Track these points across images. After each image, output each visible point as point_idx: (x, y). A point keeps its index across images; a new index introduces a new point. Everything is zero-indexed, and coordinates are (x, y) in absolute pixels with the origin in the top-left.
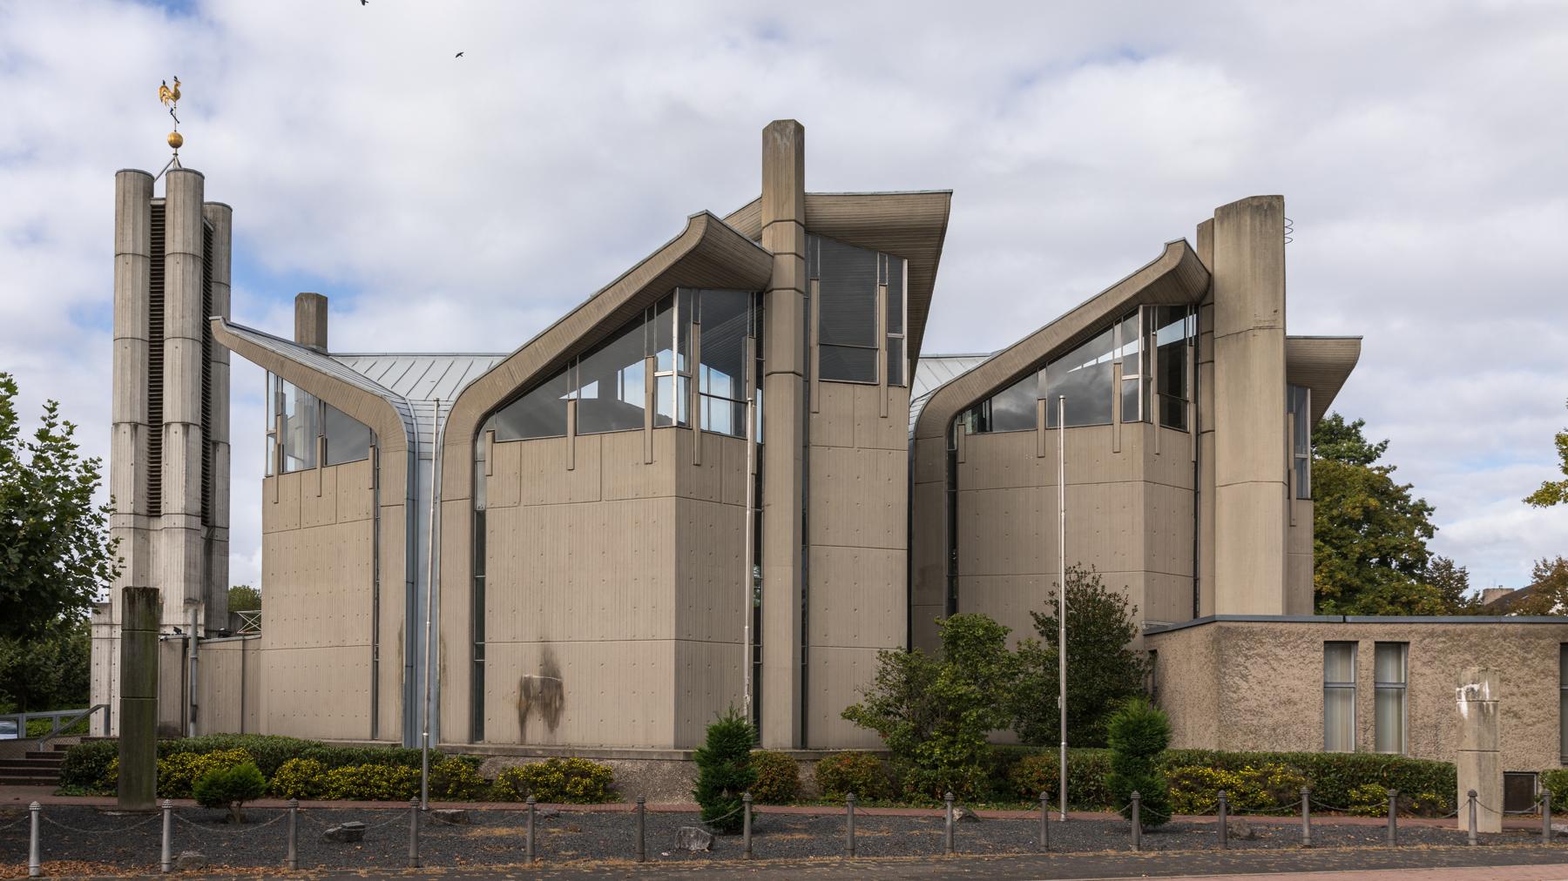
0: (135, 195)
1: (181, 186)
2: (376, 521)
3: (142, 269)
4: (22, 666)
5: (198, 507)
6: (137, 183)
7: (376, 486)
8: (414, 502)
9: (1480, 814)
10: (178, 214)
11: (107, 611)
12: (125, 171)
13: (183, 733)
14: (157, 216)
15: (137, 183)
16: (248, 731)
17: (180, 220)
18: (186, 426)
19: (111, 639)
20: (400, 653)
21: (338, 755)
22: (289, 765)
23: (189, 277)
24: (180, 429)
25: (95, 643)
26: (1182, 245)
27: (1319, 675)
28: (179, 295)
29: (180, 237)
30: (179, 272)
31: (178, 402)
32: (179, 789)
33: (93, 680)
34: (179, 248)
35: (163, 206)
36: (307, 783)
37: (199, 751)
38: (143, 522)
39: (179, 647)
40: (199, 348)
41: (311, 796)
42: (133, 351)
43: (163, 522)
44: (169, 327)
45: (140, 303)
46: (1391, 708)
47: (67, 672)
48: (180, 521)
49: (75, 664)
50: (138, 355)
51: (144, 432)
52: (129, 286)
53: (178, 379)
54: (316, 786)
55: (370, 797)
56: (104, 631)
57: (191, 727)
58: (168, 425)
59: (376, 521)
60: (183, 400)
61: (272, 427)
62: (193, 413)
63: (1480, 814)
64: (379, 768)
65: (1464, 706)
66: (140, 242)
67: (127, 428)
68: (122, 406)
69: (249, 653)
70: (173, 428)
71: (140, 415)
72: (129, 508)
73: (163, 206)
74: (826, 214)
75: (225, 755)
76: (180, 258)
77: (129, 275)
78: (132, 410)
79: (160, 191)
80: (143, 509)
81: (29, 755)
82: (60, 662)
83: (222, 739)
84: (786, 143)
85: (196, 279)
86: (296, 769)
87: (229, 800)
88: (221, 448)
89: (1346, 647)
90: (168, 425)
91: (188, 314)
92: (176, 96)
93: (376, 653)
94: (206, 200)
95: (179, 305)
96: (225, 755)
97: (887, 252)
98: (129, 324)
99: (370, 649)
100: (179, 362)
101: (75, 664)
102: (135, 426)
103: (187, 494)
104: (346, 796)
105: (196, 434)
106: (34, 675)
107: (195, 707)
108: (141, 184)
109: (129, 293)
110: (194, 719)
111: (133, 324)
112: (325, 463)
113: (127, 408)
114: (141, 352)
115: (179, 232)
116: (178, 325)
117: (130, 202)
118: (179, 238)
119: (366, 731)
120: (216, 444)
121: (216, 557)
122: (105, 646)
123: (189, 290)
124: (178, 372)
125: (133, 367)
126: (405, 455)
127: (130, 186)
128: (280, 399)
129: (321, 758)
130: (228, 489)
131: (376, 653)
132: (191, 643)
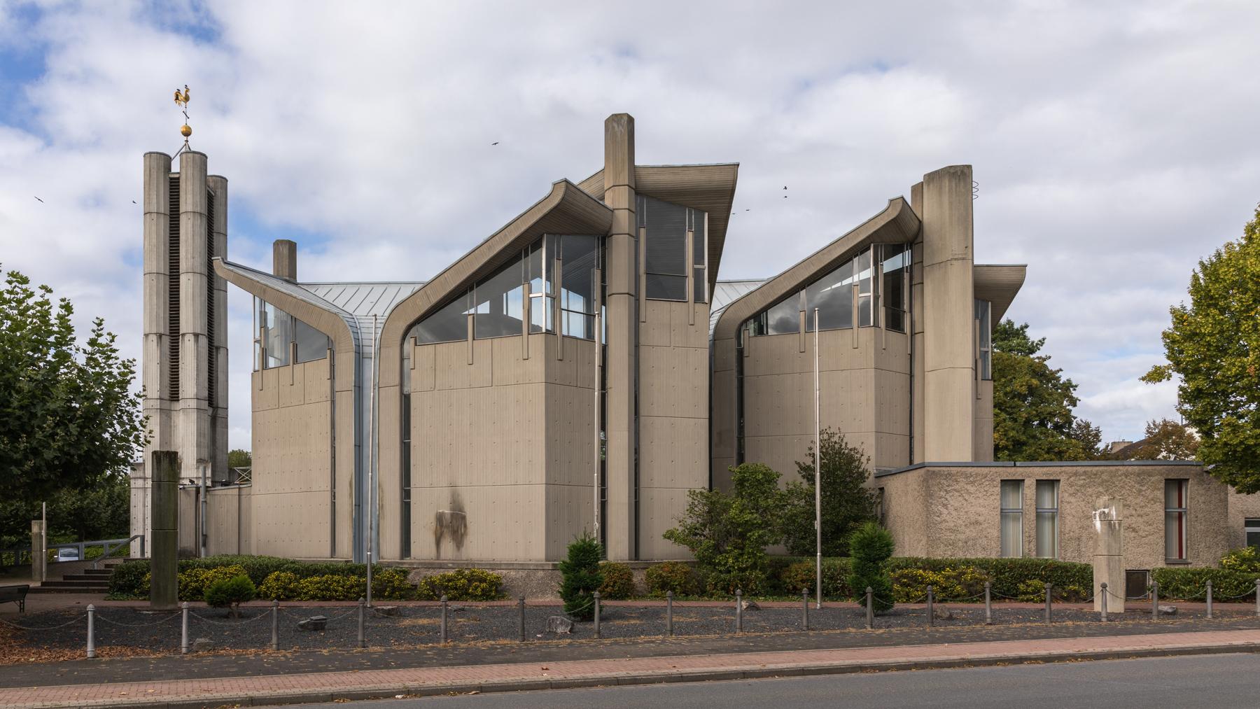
1: (191, 164)
2: (333, 402)
3: (164, 223)
4: (81, 508)
5: (206, 394)
7: (332, 377)
8: (359, 388)
9: (1109, 599)
10: (189, 183)
13: (197, 555)
14: (174, 185)
16: (243, 552)
17: (190, 188)
18: (196, 335)
19: (145, 489)
20: (351, 495)
21: (307, 569)
22: (272, 576)
23: (197, 229)
24: (192, 338)
25: (133, 492)
27: (998, 504)
28: (190, 241)
29: (190, 201)
30: (190, 225)
31: (190, 318)
32: (193, 595)
34: (190, 208)
36: (285, 589)
37: (208, 567)
38: (167, 405)
39: (193, 494)
40: (205, 280)
41: (288, 598)
42: (158, 282)
43: (181, 405)
44: (184, 265)
45: (162, 247)
46: (1047, 526)
48: (193, 404)
51: (166, 340)
52: (154, 236)
53: (190, 302)
54: (291, 591)
55: (330, 598)
56: (140, 483)
57: (203, 550)
59: (333, 402)
60: (194, 317)
61: (257, 336)
62: (201, 327)
63: (1109, 599)
64: (336, 577)
65: (1098, 524)
67: (154, 338)
68: (151, 322)
70: (187, 337)
71: (164, 328)
72: (156, 395)
74: (649, 180)
75: (227, 570)
76: (190, 215)
77: (154, 228)
78: (158, 325)
79: (175, 167)
80: (167, 396)
83: (224, 559)
84: (621, 130)
86: (277, 579)
87: (229, 603)
88: (222, 351)
89: (1014, 484)
91: (197, 256)
92: (187, 99)
93: (334, 496)
94: (209, 173)
95: (190, 249)
96: (227, 570)
97: (694, 206)
98: (154, 263)
99: (329, 494)
100: (190, 290)
102: (160, 336)
103: (198, 384)
104: (313, 598)
105: (204, 341)
107: (205, 536)
108: (162, 163)
109: (154, 241)
110: (204, 545)
111: (158, 263)
112: (296, 361)
113: (154, 324)
114: (164, 283)
115: (190, 196)
116: (190, 264)
117: (154, 175)
118: (190, 201)
120: (218, 348)
121: (219, 429)
122: (140, 494)
124: (190, 297)
126: (353, 355)
127: (154, 164)
128: (264, 316)
129: (295, 571)
131: (334, 496)
132: (202, 490)
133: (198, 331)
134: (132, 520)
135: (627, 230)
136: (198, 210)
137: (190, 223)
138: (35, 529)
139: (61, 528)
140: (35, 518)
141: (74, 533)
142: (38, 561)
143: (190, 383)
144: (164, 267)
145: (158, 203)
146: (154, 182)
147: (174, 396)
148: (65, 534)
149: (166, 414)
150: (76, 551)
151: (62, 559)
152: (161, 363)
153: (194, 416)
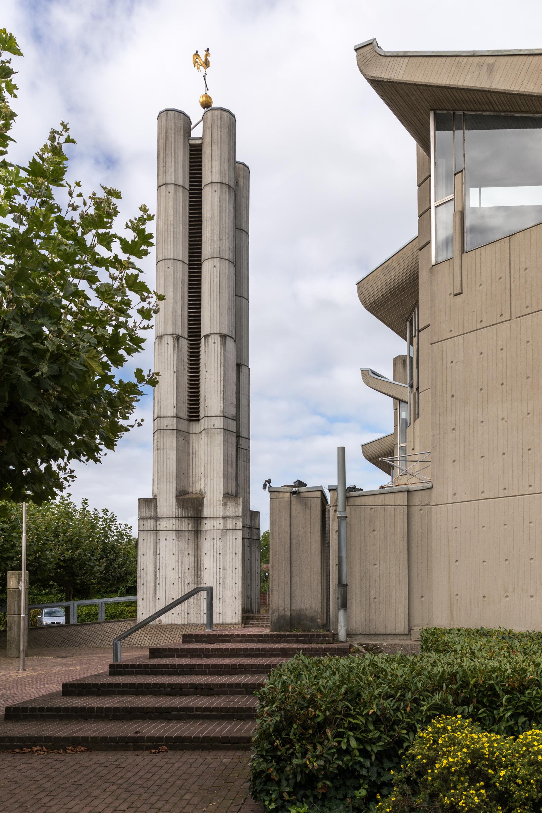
0: (177, 132)
1: (217, 123)
3: (182, 199)
4: (72, 560)
5: (232, 411)
6: (174, 122)
10: (216, 148)
11: (152, 505)
12: (167, 110)
14: (195, 153)
15: (174, 122)
17: (216, 153)
18: (223, 337)
23: (225, 204)
24: (218, 339)
26: (319, 494)
28: (216, 219)
29: (212, 171)
31: (212, 319)
33: (139, 569)
34: (216, 179)
35: (201, 145)
38: (184, 425)
42: (175, 271)
43: (203, 424)
44: (208, 247)
45: (180, 228)
47: (107, 568)
48: (219, 423)
49: (114, 560)
50: (179, 274)
51: (184, 344)
52: (171, 212)
53: (216, 294)
58: (207, 336)
60: (221, 314)
66: (180, 174)
67: (170, 340)
69: (414, 509)
70: (211, 339)
71: (182, 330)
72: (172, 412)
73: (201, 145)
76: (217, 187)
77: (171, 203)
78: (174, 324)
79: (197, 132)
80: (184, 414)
81: (155, 653)
82: (102, 558)
85: (228, 207)
90: (207, 336)
91: (225, 237)
92: (207, 64)
98: (171, 247)
100: (216, 280)
101: (114, 560)
102: (177, 338)
103: (225, 398)
106: (81, 569)
108: (181, 123)
109: (171, 219)
110: (344, 605)
113: (170, 322)
115: (216, 164)
116: (216, 247)
117: (172, 138)
119: (204, 620)
123: (225, 215)
124: (216, 288)
125: (175, 285)
127: (172, 124)
130: (249, 406)
133: (225, 332)
134: (140, 573)
135: (105, 511)
136: (226, 180)
137: (216, 196)
138: (12, 583)
139: (45, 585)
140: (13, 569)
141: (61, 591)
142: (15, 628)
143: (213, 399)
144: (182, 253)
145: (176, 171)
146: (171, 146)
147: (194, 414)
148: (49, 593)
149: (183, 437)
150: (392, 698)
151: (47, 621)
152: (178, 372)
153: (219, 438)
